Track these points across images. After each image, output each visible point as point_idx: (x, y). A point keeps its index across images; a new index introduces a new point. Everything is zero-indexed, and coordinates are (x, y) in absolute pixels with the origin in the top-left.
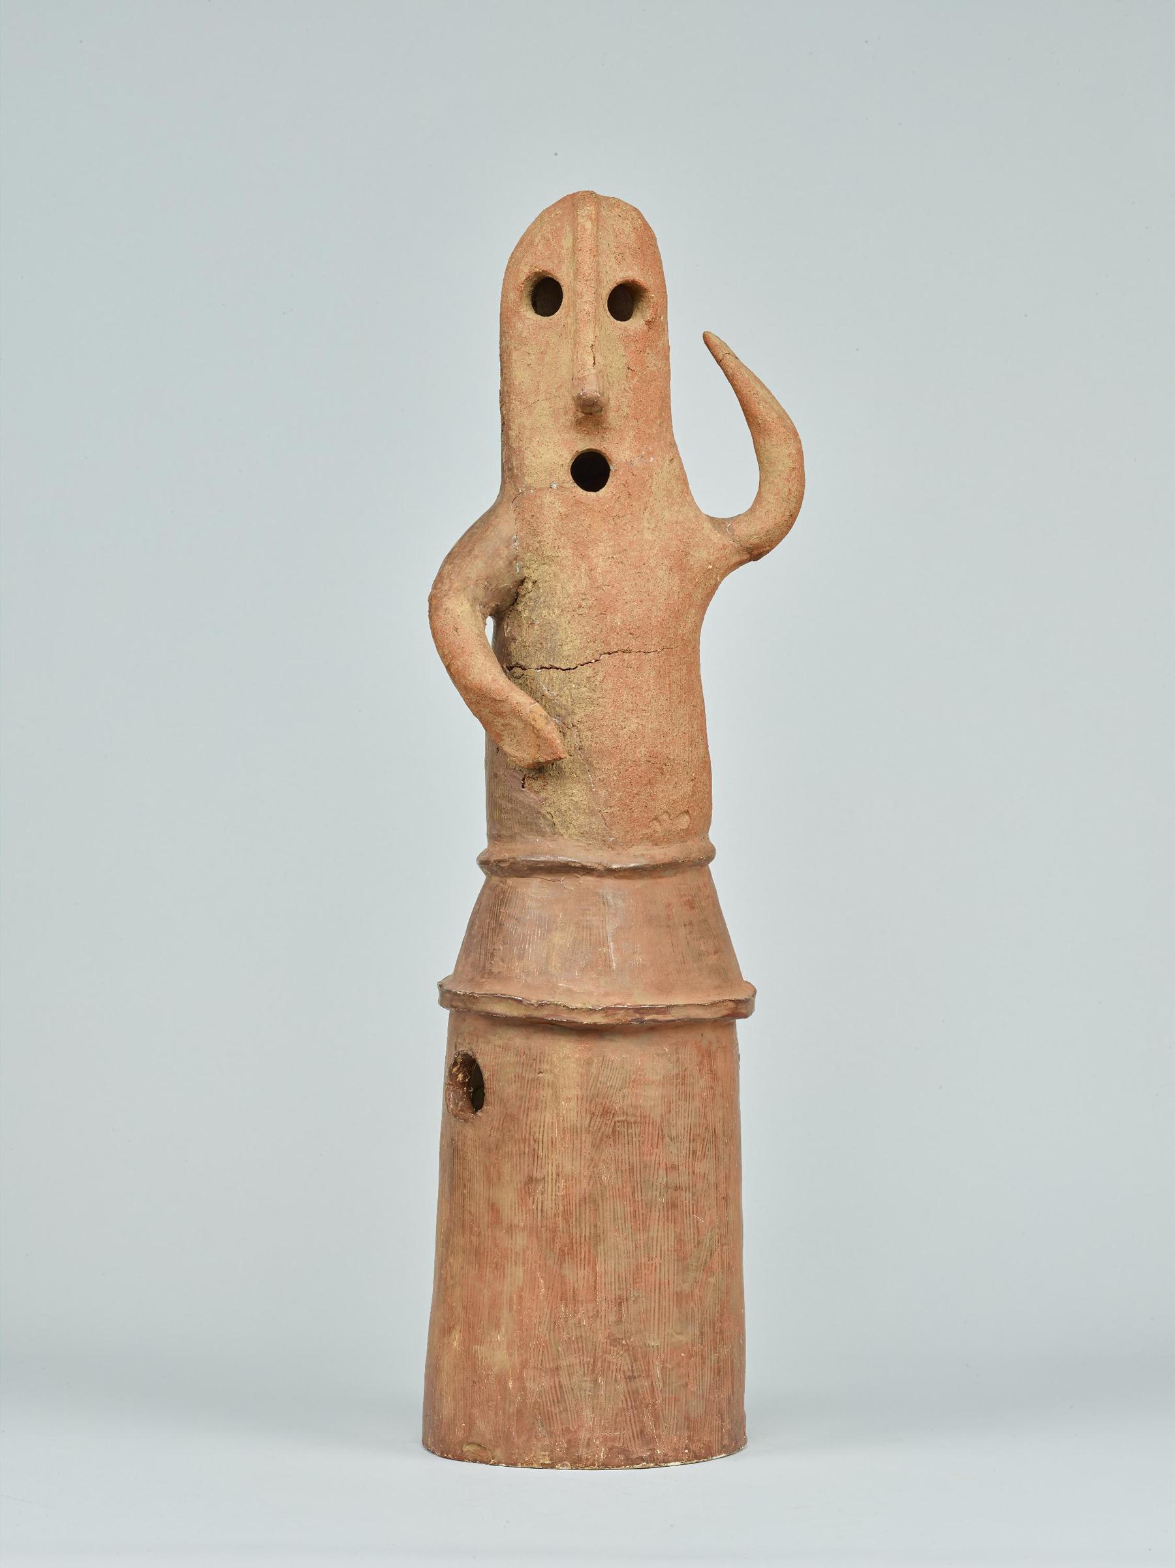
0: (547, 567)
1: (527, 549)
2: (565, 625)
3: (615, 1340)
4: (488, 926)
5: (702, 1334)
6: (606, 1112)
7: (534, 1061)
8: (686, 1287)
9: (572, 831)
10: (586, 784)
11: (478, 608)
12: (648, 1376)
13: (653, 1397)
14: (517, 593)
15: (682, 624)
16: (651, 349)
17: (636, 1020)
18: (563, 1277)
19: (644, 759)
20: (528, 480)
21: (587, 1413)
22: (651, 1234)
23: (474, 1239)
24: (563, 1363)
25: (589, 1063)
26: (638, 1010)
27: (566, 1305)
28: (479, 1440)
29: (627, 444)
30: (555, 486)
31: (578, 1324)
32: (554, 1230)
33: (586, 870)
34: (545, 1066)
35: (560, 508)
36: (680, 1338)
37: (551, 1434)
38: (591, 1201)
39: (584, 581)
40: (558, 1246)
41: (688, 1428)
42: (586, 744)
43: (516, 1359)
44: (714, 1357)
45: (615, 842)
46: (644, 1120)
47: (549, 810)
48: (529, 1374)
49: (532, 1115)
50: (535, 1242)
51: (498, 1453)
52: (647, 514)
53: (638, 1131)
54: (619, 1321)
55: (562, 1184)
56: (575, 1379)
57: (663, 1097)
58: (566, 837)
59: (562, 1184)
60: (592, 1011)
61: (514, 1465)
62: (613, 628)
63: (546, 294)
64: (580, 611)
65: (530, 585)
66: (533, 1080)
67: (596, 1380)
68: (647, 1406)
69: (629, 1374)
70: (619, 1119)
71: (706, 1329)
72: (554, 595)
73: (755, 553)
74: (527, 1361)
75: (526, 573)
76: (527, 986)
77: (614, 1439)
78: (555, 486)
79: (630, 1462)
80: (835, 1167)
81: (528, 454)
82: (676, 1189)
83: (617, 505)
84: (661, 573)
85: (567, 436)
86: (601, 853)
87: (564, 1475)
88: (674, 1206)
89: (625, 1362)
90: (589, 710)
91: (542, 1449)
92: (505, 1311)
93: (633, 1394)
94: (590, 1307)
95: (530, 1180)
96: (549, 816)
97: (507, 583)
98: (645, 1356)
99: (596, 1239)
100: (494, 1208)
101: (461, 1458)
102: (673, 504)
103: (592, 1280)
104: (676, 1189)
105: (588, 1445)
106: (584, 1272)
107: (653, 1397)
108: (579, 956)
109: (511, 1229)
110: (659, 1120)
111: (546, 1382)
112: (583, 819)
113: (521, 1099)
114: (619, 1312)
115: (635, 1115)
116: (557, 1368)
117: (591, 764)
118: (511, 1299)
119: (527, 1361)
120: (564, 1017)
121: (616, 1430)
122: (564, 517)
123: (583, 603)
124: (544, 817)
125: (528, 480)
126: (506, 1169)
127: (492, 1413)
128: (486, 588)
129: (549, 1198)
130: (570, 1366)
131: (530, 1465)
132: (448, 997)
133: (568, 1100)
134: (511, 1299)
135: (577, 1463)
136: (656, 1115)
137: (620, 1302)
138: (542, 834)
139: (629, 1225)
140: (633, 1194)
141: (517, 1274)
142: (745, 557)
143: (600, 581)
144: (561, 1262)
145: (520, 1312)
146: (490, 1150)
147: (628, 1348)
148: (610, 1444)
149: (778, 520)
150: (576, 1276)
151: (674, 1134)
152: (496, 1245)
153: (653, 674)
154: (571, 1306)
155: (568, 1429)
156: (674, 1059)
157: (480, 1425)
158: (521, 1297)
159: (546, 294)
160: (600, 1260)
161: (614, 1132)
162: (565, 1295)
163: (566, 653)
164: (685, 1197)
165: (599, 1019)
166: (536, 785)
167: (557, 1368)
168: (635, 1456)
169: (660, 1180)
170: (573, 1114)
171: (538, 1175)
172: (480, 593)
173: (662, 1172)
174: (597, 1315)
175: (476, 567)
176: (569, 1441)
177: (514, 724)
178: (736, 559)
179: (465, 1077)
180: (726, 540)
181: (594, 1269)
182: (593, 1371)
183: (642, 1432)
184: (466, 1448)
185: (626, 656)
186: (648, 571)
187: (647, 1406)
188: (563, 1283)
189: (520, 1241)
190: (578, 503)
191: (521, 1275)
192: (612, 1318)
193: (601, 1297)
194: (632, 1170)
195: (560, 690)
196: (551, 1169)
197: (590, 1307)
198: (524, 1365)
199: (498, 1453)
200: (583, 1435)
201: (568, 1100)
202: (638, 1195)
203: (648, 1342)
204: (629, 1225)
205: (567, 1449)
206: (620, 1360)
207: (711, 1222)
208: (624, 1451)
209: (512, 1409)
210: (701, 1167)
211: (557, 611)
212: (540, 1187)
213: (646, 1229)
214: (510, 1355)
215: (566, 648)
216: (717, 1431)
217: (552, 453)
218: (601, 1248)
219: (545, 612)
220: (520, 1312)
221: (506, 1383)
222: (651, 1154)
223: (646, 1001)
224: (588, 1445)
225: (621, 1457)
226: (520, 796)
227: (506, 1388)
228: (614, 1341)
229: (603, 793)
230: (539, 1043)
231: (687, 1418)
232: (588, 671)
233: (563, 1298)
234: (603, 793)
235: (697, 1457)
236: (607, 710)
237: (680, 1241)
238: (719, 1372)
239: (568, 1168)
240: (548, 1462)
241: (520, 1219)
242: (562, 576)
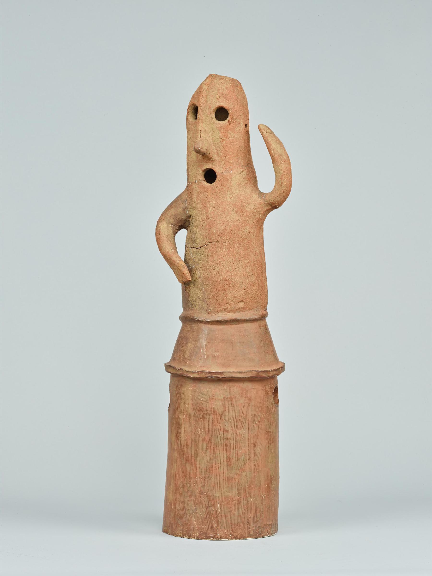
2: (198, 232)
3: (202, 492)
5: (239, 493)
6: (200, 409)
8: (231, 475)
9: (197, 307)
11: (170, 226)
12: (214, 507)
15: (241, 232)
16: (231, 131)
17: (209, 376)
18: (186, 468)
22: (216, 455)
24: (186, 500)
25: (195, 391)
26: (210, 373)
29: (221, 166)
32: (184, 451)
33: (201, 322)
34: (182, 392)
36: (228, 494)
37: (182, 525)
38: (195, 441)
39: (204, 216)
41: (231, 527)
42: (202, 275)
44: (245, 502)
46: (215, 413)
49: (179, 409)
52: (229, 192)
53: (212, 417)
54: (204, 486)
55: (186, 435)
56: (189, 506)
57: (223, 405)
64: (202, 227)
65: (192, 217)
67: (196, 507)
68: (214, 518)
69: (207, 505)
70: (205, 412)
71: (241, 491)
75: (190, 213)
77: (202, 529)
79: (207, 538)
82: (227, 439)
87: (186, 540)
88: (226, 445)
89: (206, 501)
91: (180, 531)
93: (209, 513)
94: (194, 480)
95: (178, 433)
97: (184, 217)
98: (214, 499)
99: (196, 455)
102: (240, 188)
103: (195, 470)
104: (227, 439)
105: (193, 530)
107: (216, 514)
110: (220, 413)
112: (201, 303)
114: (204, 482)
115: (211, 411)
121: (202, 525)
123: (204, 224)
128: (174, 219)
132: (168, 367)
133: (188, 404)
135: (190, 537)
136: (220, 412)
137: (205, 479)
139: (208, 451)
140: (210, 440)
142: (270, 207)
143: (210, 216)
144: (186, 464)
147: (207, 496)
148: (200, 530)
151: (227, 419)
153: (227, 250)
154: (188, 479)
156: (228, 391)
159: (195, 110)
161: (203, 417)
164: (232, 442)
165: (196, 376)
169: (220, 435)
170: (190, 409)
171: (180, 431)
172: (172, 220)
173: (221, 433)
174: (196, 483)
175: (173, 212)
176: (187, 528)
178: (266, 208)
181: (196, 466)
183: (212, 527)
185: (217, 244)
186: (228, 213)
187: (214, 518)
190: (204, 188)
192: (201, 485)
194: (209, 431)
196: (183, 429)
200: (192, 526)
202: (212, 440)
203: (215, 494)
204: (208, 451)
205: (187, 531)
207: (245, 452)
208: (205, 533)
210: (239, 432)
211: (196, 227)
213: (215, 453)
215: (197, 240)
218: (198, 459)
222: (217, 426)
223: (214, 369)
224: (193, 530)
225: (204, 535)
229: (207, 293)
231: (231, 523)
235: (236, 538)
236: (225, 265)
237: (229, 458)
238: (247, 508)
239: (188, 429)
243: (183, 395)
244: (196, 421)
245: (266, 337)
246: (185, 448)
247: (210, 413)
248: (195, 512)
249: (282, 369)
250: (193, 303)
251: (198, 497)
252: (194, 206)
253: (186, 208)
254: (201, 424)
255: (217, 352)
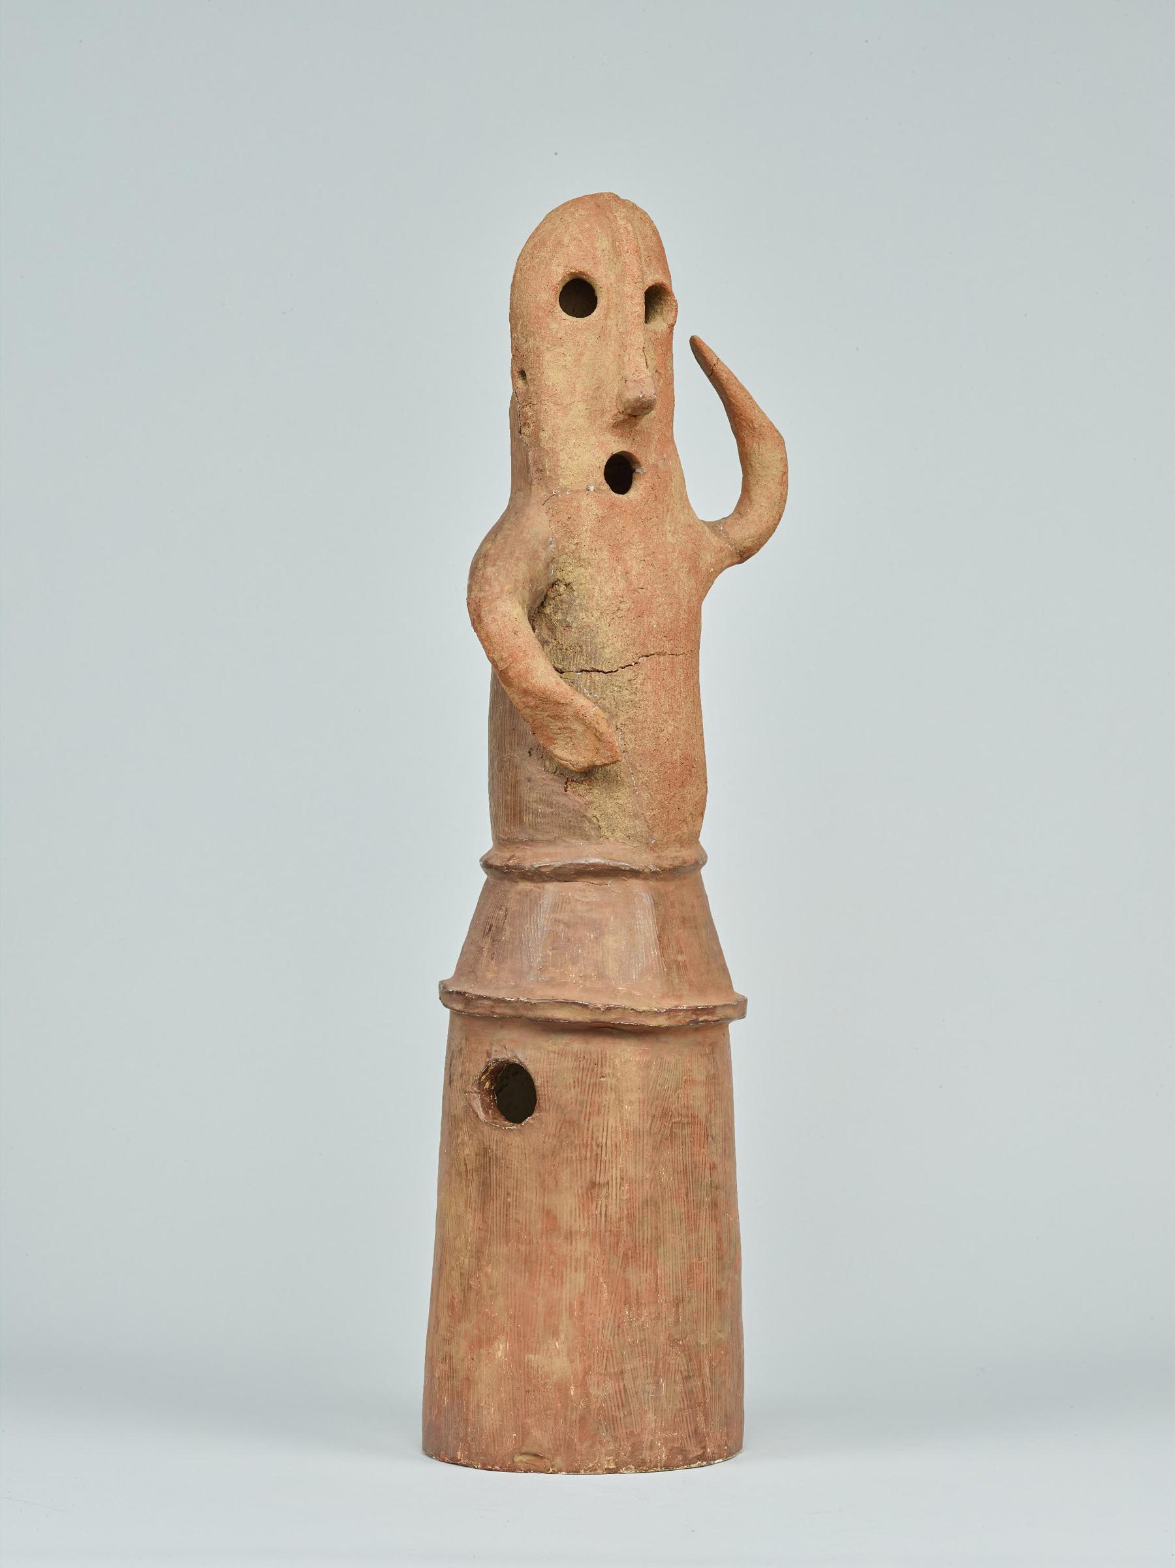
0: (583, 570)
1: (562, 551)
4: (489, 932)
6: (665, 1114)
7: (593, 1069)
9: (618, 834)
10: (630, 787)
12: (700, 1376)
13: (704, 1395)
14: (546, 597)
18: (626, 1282)
19: (679, 761)
20: (563, 482)
21: (650, 1416)
23: (522, 1248)
24: (628, 1367)
27: (630, 1309)
28: (535, 1450)
30: (592, 488)
31: (642, 1328)
32: (618, 1235)
34: (607, 1070)
35: (596, 510)
37: (616, 1439)
40: (621, 1250)
43: (579, 1366)
45: (656, 845)
46: (694, 1120)
47: (595, 813)
48: (593, 1379)
50: (598, 1246)
51: (558, 1461)
54: (677, 1323)
55: (626, 1187)
56: (639, 1382)
58: (612, 840)
59: (626, 1187)
60: (658, 1013)
61: (577, 1472)
62: (650, 631)
63: (579, 296)
64: (619, 614)
65: (562, 588)
66: (595, 1084)
69: (685, 1374)
70: (677, 1119)
72: (591, 597)
73: (743, 555)
74: (590, 1366)
75: (559, 575)
76: (585, 990)
77: (674, 1440)
78: (592, 488)
79: (687, 1463)
80: (833, 1159)
81: (563, 456)
83: (646, 508)
84: (682, 576)
85: (602, 438)
86: (645, 856)
90: (632, 712)
92: (565, 1316)
93: (689, 1394)
94: (653, 1309)
95: (593, 1185)
96: (594, 820)
97: (542, 587)
98: (698, 1355)
99: (658, 1240)
100: (549, 1215)
101: (512, 1469)
106: (647, 1275)
107: (704, 1395)
108: (610, 956)
109: (570, 1236)
111: (610, 1386)
112: (628, 822)
113: (582, 1104)
116: (622, 1373)
117: (634, 767)
118: (571, 1305)
119: (590, 1366)
120: (632, 1020)
122: (602, 520)
123: (622, 606)
124: (590, 821)
125: (563, 482)
126: (565, 1176)
127: (550, 1423)
129: (613, 1202)
130: (635, 1369)
131: (593, 1471)
133: (631, 1103)
134: (571, 1305)
135: (642, 1466)
138: (587, 838)
141: (577, 1280)
143: (635, 581)
145: (581, 1318)
146: (544, 1156)
149: (524, 519)
150: (638, 1279)
152: (552, 1252)
155: (632, 1432)
157: (536, 1434)
158: (582, 1303)
160: (660, 1261)
162: (627, 1299)
163: (608, 656)
165: (662, 1021)
166: (582, 789)
167: (622, 1373)
168: (691, 1456)
171: (601, 1179)
174: (658, 1317)
177: (574, 727)
179: (491, 1085)
180: (722, 544)
182: (655, 1374)
184: (518, 1459)
185: (662, 659)
188: (627, 1287)
189: (581, 1247)
190: (613, 505)
191: (582, 1280)
192: (671, 1320)
193: (662, 1298)
194: (685, 1171)
195: (603, 692)
196: (615, 1173)
197: (653, 1309)
198: (586, 1372)
199: (558, 1461)
200: (647, 1438)
201: (631, 1103)
202: (690, 1195)
205: (632, 1452)
206: (678, 1361)
209: (575, 1416)
212: (604, 1192)
213: (697, 1229)
214: (572, 1362)
215: (607, 651)
216: (706, 1429)
217: (582, 455)
218: (661, 1250)
219: (582, 615)
220: (581, 1318)
221: (568, 1390)
225: (680, 1457)
226: (563, 800)
227: (567, 1395)
228: (673, 1342)
229: (645, 796)
230: (597, 1046)
232: (628, 674)
233: (627, 1302)
234: (645, 796)
239: (631, 1172)
240: (612, 1466)
241: (580, 1225)
242: (599, 579)
243: (609, 1081)
244: (654, 1148)
245: (699, 922)
246: (624, 1223)
247: (685, 1120)
248: (657, 1398)
249: (740, 1008)
250: (602, 824)
251: (665, 1354)
252: (584, 555)
253: (553, 560)
254: (667, 1154)
255: (682, 952)
